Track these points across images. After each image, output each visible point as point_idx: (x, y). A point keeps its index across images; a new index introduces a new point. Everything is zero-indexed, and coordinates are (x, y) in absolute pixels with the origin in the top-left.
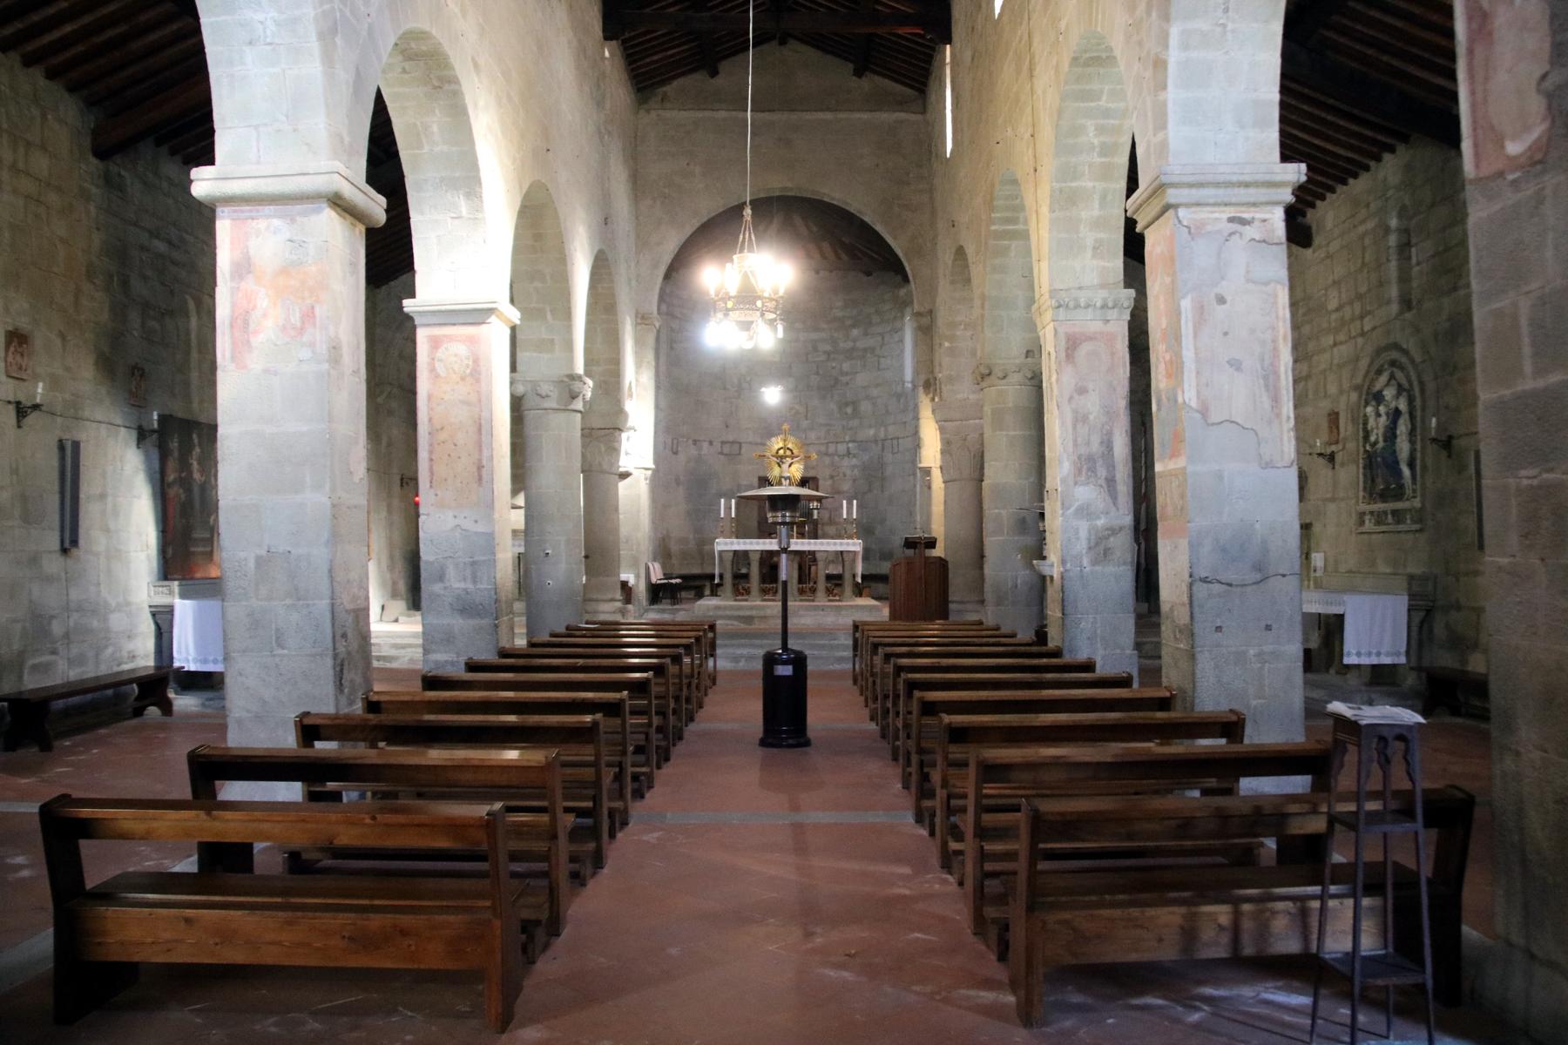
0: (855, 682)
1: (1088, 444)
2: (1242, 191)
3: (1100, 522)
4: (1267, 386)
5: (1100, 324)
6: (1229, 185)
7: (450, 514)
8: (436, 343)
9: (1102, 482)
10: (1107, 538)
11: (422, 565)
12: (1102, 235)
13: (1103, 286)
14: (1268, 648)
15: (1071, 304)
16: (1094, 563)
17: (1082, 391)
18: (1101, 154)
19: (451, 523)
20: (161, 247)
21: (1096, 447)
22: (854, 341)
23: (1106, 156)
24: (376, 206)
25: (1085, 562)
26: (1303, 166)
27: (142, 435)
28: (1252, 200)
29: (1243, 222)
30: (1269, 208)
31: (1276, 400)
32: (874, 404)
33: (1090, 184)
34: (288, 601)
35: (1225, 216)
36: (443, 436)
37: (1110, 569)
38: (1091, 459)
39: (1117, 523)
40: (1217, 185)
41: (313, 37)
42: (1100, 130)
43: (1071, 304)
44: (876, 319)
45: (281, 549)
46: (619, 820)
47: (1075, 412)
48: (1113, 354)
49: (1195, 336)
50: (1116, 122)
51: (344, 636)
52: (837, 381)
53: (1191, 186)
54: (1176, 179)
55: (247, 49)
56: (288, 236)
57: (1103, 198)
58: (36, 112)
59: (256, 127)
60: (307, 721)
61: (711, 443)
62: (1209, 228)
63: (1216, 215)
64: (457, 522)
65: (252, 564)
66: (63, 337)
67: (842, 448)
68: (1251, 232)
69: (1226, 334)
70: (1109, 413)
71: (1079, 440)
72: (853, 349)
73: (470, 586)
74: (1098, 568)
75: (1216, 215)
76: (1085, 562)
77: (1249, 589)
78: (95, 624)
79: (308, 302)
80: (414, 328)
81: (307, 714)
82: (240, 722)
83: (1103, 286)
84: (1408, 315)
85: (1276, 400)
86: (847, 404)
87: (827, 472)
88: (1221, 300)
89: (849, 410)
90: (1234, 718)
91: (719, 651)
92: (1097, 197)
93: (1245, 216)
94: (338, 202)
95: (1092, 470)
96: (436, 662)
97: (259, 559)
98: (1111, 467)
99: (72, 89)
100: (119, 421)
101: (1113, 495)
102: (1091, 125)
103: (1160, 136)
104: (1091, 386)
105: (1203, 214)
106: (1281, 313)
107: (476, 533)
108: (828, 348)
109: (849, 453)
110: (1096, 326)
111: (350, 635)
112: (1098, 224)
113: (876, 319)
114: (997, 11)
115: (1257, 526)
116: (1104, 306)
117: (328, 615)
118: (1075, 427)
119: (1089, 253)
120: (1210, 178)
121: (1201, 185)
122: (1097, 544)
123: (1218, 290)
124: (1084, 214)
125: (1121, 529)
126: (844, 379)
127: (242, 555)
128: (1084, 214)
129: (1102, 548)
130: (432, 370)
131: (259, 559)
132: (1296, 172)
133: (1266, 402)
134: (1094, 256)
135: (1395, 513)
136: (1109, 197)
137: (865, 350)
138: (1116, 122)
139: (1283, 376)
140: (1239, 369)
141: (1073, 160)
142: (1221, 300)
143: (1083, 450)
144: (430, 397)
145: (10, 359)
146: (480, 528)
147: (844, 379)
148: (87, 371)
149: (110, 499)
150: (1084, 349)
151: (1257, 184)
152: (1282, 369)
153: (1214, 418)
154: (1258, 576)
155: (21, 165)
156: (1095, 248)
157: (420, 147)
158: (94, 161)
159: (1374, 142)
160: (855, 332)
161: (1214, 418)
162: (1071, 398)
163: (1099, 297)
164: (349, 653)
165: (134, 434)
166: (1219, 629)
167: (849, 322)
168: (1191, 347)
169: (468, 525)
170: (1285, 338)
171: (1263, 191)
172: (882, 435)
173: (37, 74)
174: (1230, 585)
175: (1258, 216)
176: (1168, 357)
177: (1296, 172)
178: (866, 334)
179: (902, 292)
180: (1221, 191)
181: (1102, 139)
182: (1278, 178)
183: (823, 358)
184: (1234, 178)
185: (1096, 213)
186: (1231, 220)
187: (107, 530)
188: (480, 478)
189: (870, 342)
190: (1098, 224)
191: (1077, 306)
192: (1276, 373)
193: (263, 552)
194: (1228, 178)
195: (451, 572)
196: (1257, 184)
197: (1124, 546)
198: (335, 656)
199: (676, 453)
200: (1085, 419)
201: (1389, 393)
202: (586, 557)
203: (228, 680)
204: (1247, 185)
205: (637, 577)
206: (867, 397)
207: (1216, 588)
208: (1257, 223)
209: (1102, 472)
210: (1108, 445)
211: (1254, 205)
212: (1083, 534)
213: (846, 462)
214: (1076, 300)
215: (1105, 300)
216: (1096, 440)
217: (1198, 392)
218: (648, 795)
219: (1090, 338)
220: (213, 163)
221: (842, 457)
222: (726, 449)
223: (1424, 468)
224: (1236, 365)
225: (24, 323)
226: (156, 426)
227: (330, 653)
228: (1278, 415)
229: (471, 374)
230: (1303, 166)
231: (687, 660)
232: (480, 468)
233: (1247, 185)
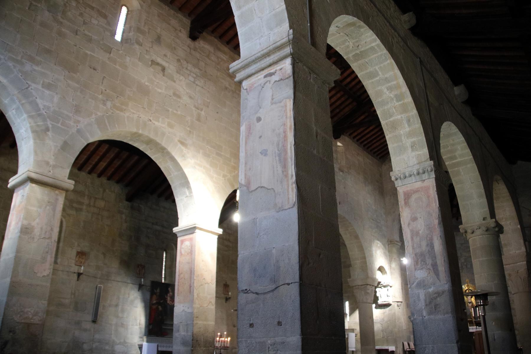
1: (420, 246)
3: (431, 290)
4: (280, 160)
5: (420, 183)
7: (182, 305)
8: (182, 242)
9: (430, 266)
10: (435, 298)
12: (414, 139)
14: (278, 339)
15: (402, 176)
16: (430, 313)
17: (414, 219)
18: (397, 101)
19: (182, 308)
20: (158, 228)
21: (424, 248)
23: (400, 101)
25: (425, 314)
27: (141, 287)
29: (271, 75)
31: (285, 167)
33: (399, 117)
35: (263, 76)
36: (182, 276)
37: (439, 317)
38: (422, 255)
39: (441, 289)
41: (30, 132)
42: (390, 89)
43: (402, 176)
47: (412, 231)
48: (428, 197)
50: (395, 83)
57: (409, 121)
58: (101, 190)
62: (255, 85)
63: (259, 77)
66: (104, 254)
69: (260, 137)
70: (429, 228)
71: (415, 245)
73: (186, 334)
74: (432, 317)
75: (259, 77)
76: (425, 314)
77: (268, 296)
78: (107, 348)
80: (177, 238)
85: (285, 167)
88: (259, 119)
92: (405, 122)
93: (272, 71)
95: (424, 261)
98: (434, 257)
99: (118, 182)
100: (129, 281)
102: (384, 88)
104: (418, 215)
106: (288, 115)
107: (189, 313)
110: (419, 184)
112: (410, 135)
115: (274, 251)
116: (418, 174)
119: (410, 149)
122: (430, 303)
123: (259, 115)
125: (443, 292)
128: (401, 132)
133: (280, 169)
134: (413, 151)
136: (411, 120)
138: (395, 83)
139: (289, 151)
141: (386, 107)
143: (418, 251)
144: (179, 262)
145: (77, 259)
146: (189, 310)
148: (115, 265)
149: (120, 307)
150: (414, 197)
154: (274, 287)
155: (92, 204)
156: (412, 147)
157: (171, 175)
158: (127, 203)
162: (409, 224)
165: (137, 286)
166: (251, 325)
168: (244, 151)
169: (186, 310)
170: (290, 129)
173: (104, 180)
174: (257, 293)
181: (393, 93)
185: (408, 129)
186: (265, 77)
187: (117, 317)
188: (190, 292)
190: (410, 135)
191: (405, 177)
195: (181, 328)
197: (445, 302)
200: (417, 233)
205: (396, 348)
207: (251, 296)
209: (429, 261)
210: (431, 245)
212: (422, 297)
214: (404, 174)
215: (418, 170)
216: (424, 244)
217: (245, 174)
219: (416, 191)
224: (264, 153)
225: (86, 249)
228: (286, 176)
232: (190, 287)
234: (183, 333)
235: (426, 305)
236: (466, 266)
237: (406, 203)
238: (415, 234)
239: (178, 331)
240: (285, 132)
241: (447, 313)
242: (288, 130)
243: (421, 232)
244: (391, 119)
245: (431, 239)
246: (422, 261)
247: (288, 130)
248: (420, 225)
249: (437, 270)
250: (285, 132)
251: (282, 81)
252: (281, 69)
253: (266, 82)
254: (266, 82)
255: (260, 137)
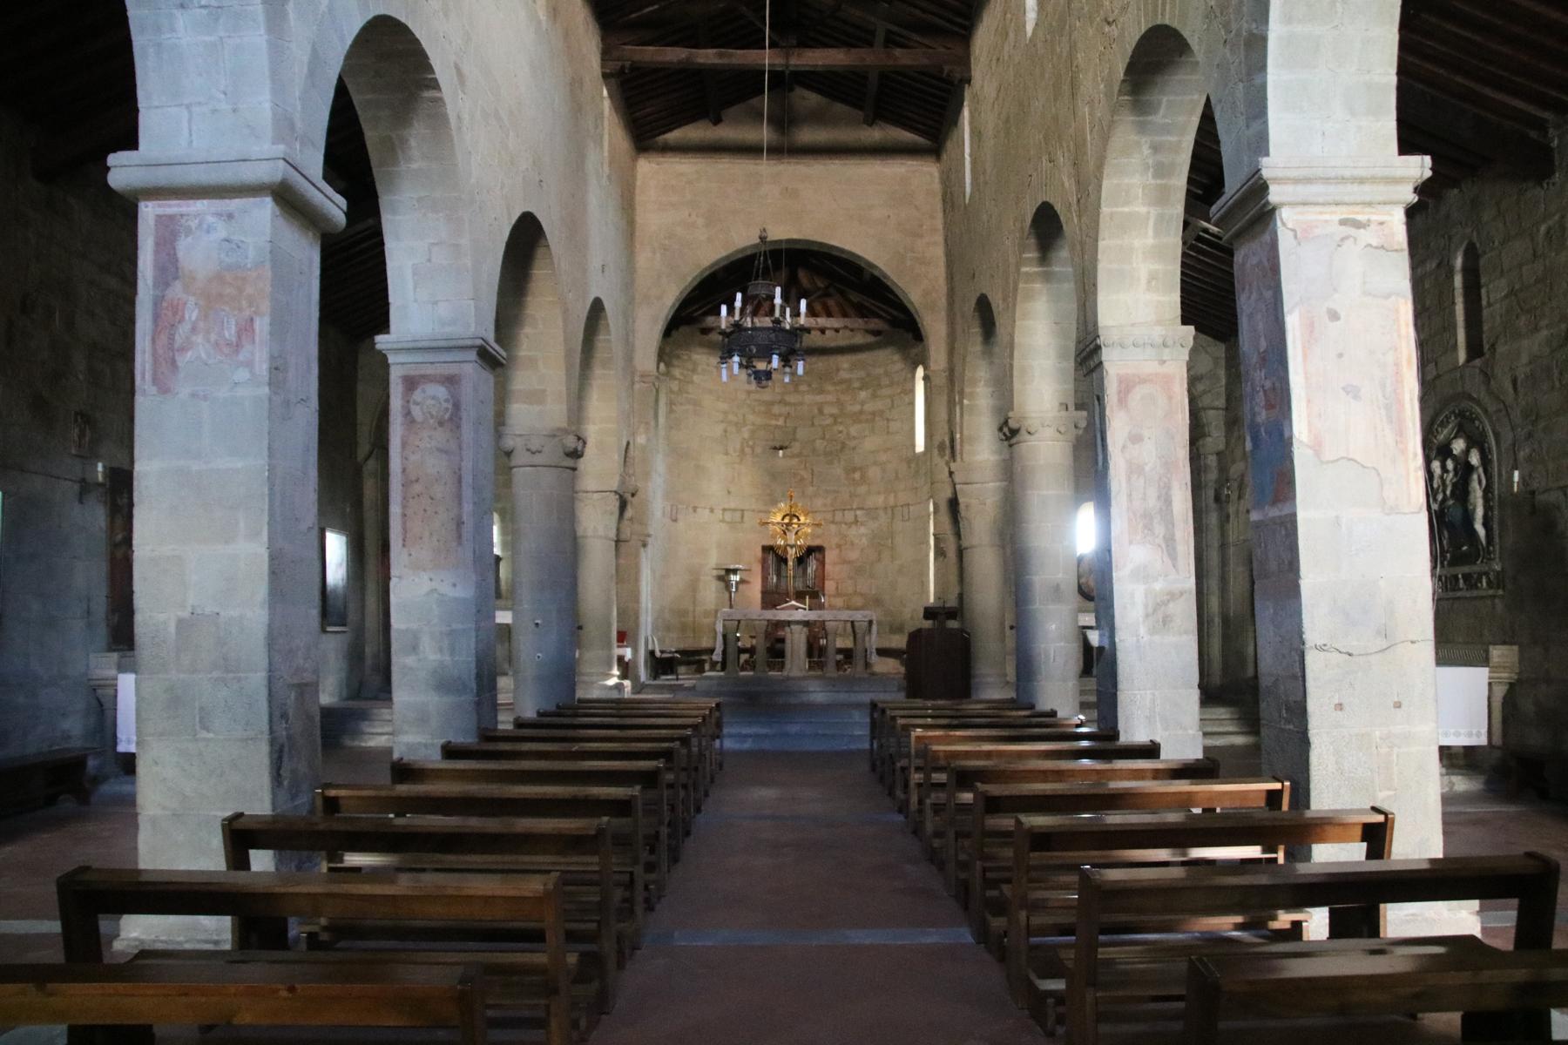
0: (873, 768)
2: (1356, 188)
3: (1158, 586)
6: (1343, 180)
9: (1160, 540)
11: (393, 634)
13: (1159, 322)
16: (1153, 631)
17: (1136, 439)
21: (1153, 502)
22: (863, 403)
24: (334, 207)
25: (1142, 631)
26: (1428, 159)
28: (1368, 199)
29: (1358, 225)
30: (1388, 207)
31: (1401, 433)
32: (884, 471)
34: (215, 674)
35: (1336, 218)
37: (1171, 639)
38: (1147, 517)
40: (1326, 180)
44: (885, 381)
45: (208, 610)
46: (627, 949)
48: (1170, 398)
49: (1305, 356)
51: (284, 716)
52: (844, 445)
53: (1297, 181)
54: (1280, 173)
55: (178, 13)
56: (224, 234)
59: (188, 107)
60: (237, 825)
61: (712, 510)
62: (1317, 231)
63: (1327, 217)
64: (434, 585)
65: (172, 629)
67: (849, 516)
68: (1366, 236)
69: (1340, 355)
72: (861, 412)
74: (1157, 638)
75: (1327, 217)
78: (21, 700)
79: (247, 313)
81: (240, 815)
82: (154, 821)
83: (1159, 322)
84: (1477, 362)
86: (854, 470)
87: (835, 541)
88: (1334, 316)
89: (857, 475)
90: (1381, 818)
91: (725, 731)
93: (1360, 217)
94: (287, 198)
95: (1148, 527)
96: (407, 744)
97: (180, 622)
101: (1172, 555)
103: (1255, 126)
104: (1146, 433)
105: (1311, 215)
106: (1403, 332)
107: (456, 599)
108: (835, 411)
109: (856, 521)
110: (1151, 367)
111: (291, 712)
113: (885, 381)
114: (1029, 28)
117: (264, 693)
118: (1129, 479)
120: (1320, 172)
121: (1308, 180)
122: (1155, 610)
124: (1137, 243)
126: (852, 444)
127: (162, 617)
128: (1137, 243)
129: (1160, 616)
130: (407, 414)
131: (180, 622)
132: (1419, 167)
135: (1467, 577)
137: (873, 414)
139: (1408, 406)
140: (1356, 397)
142: (1334, 316)
147: (852, 444)
150: (1138, 393)
151: (1373, 180)
152: (1407, 397)
153: (1328, 456)
154: (1385, 644)
159: (559, 715)
160: (863, 394)
161: (1328, 455)
162: (1124, 447)
163: (1157, 333)
164: (289, 737)
167: (856, 385)
170: (1409, 362)
171: (1382, 188)
172: (891, 501)
175: (1374, 218)
176: (1268, 384)
177: (1419, 167)
178: (874, 396)
179: (914, 351)
180: (1332, 189)
182: (1399, 173)
183: (829, 421)
184: (1347, 173)
186: (1343, 222)
189: (878, 405)
192: (1400, 403)
193: (185, 614)
194: (1341, 172)
196: (1373, 180)
198: (272, 742)
199: (675, 520)
201: (1458, 446)
202: (580, 628)
203: (142, 768)
204: (1361, 181)
205: (635, 651)
206: (875, 463)
207: (1335, 657)
208: (1373, 227)
211: (1370, 204)
213: (853, 531)
218: (658, 907)
219: (1143, 380)
220: (136, 148)
221: (849, 525)
222: (728, 517)
223: (1502, 523)
224: (1353, 392)
226: (100, 478)
227: (266, 736)
228: (1404, 452)
229: (451, 419)
230: (1428, 159)
231: (694, 741)
233: (1361, 181)
234: (432, 657)
235: (1147, 616)
236: (753, 448)
237: (1123, 401)
238: (1135, 469)
239: (414, 648)
240: (1397, 365)
241: (1186, 632)
242: (1404, 363)
243: (1147, 468)
244: (1126, 209)
245: (1168, 487)
246: (1145, 527)
247: (1404, 363)
248: (1148, 454)
249: (1174, 549)
250: (1397, 365)
251: (1382, 252)
252: (1382, 223)
253: (1347, 238)
254: (1347, 238)
255: (1340, 355)
